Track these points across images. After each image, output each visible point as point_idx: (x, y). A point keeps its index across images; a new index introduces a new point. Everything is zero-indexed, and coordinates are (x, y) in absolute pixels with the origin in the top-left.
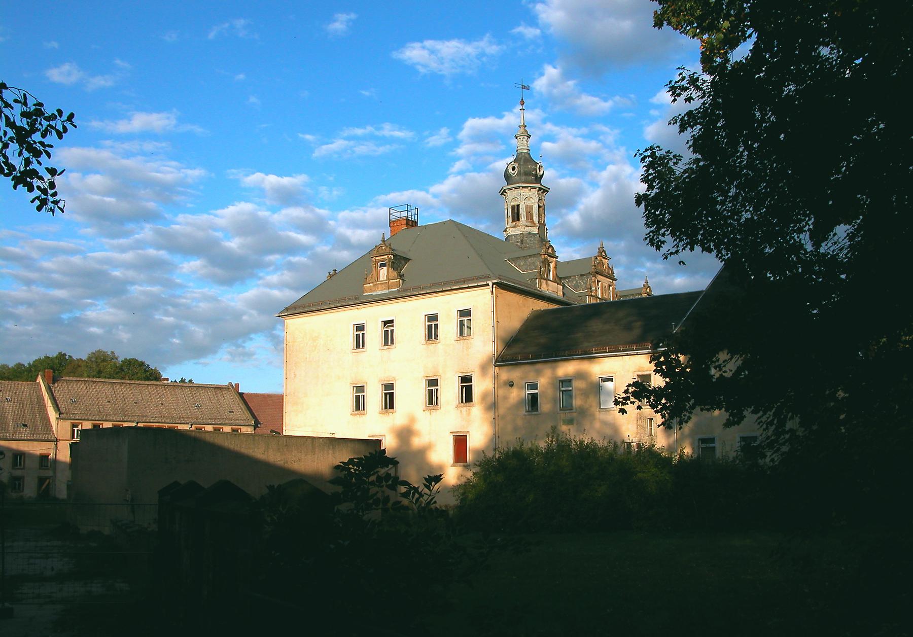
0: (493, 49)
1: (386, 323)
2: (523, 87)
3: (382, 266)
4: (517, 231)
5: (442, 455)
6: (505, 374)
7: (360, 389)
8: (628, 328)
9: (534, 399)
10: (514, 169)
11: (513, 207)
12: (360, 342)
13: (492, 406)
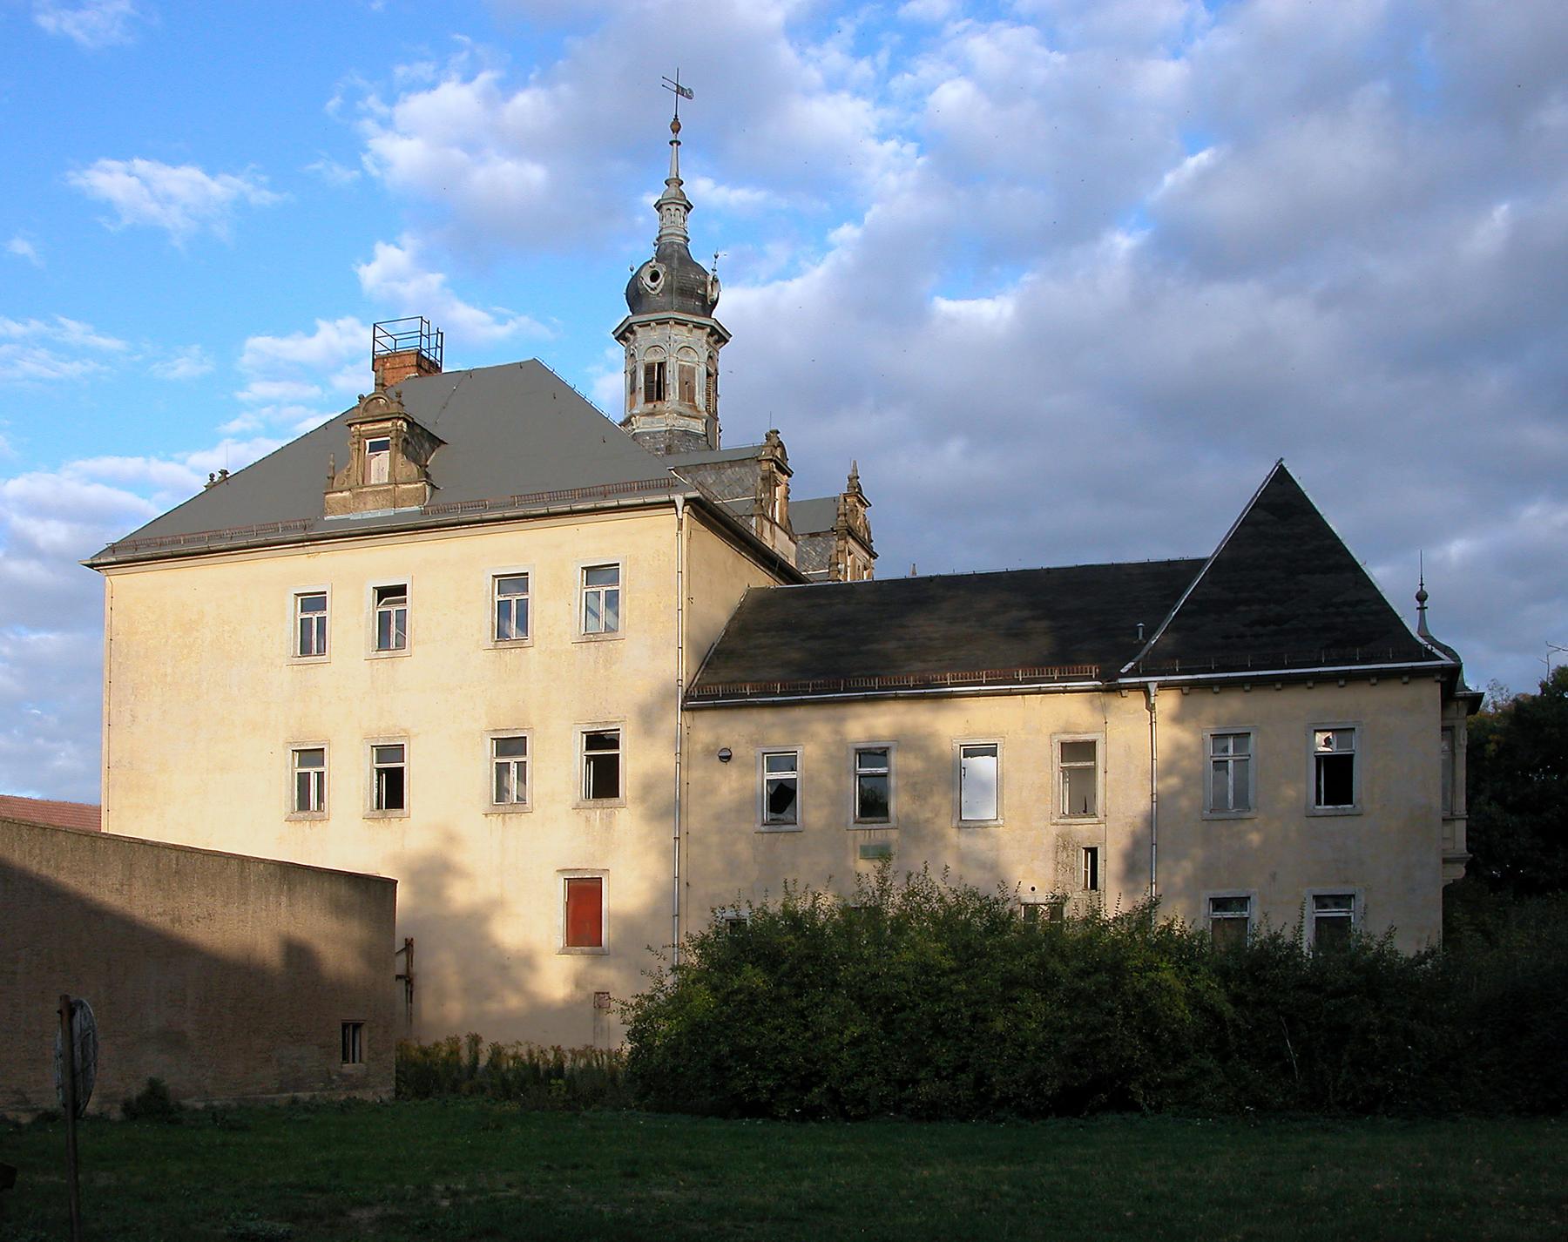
0: (264, 198)
1: (384, 593)
2: (680, 91)
3: (376, 447)
4: (659, 425)
5: (533, 926)
6: (711, 729)
7: (312, 756)
8: (1016, 634)
9: (782, 798)
10: (655, 277)
11: (649, 369)
12: (311, 640)
13: (671, 809)
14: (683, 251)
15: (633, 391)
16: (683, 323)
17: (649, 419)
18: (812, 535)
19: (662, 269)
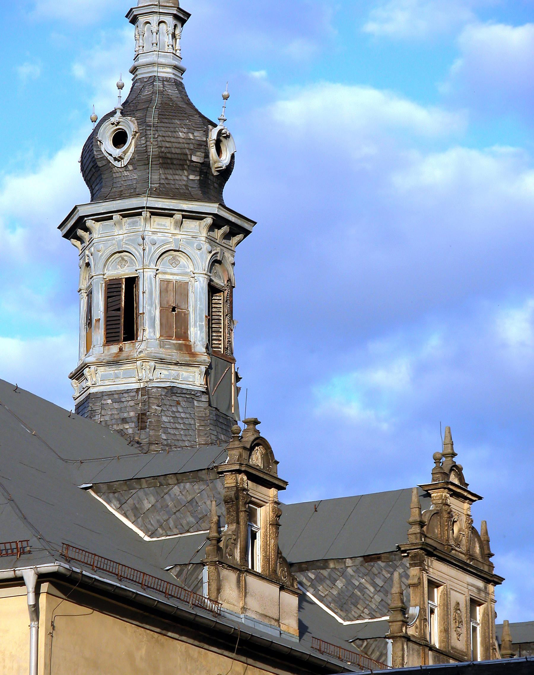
10: (120, 139)
11: (112, 288)
14: (172, 91)
15: (89, 323)
16: (167, 213)
17: (111, 371)
18: (369, 558)
19: (130, 126)
